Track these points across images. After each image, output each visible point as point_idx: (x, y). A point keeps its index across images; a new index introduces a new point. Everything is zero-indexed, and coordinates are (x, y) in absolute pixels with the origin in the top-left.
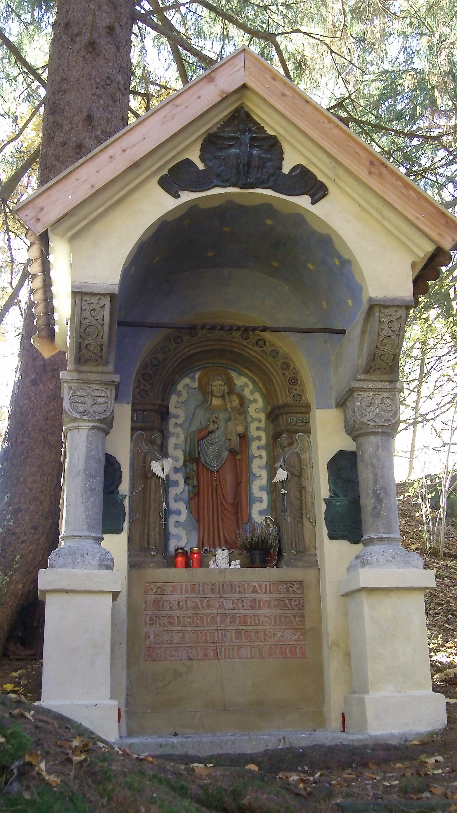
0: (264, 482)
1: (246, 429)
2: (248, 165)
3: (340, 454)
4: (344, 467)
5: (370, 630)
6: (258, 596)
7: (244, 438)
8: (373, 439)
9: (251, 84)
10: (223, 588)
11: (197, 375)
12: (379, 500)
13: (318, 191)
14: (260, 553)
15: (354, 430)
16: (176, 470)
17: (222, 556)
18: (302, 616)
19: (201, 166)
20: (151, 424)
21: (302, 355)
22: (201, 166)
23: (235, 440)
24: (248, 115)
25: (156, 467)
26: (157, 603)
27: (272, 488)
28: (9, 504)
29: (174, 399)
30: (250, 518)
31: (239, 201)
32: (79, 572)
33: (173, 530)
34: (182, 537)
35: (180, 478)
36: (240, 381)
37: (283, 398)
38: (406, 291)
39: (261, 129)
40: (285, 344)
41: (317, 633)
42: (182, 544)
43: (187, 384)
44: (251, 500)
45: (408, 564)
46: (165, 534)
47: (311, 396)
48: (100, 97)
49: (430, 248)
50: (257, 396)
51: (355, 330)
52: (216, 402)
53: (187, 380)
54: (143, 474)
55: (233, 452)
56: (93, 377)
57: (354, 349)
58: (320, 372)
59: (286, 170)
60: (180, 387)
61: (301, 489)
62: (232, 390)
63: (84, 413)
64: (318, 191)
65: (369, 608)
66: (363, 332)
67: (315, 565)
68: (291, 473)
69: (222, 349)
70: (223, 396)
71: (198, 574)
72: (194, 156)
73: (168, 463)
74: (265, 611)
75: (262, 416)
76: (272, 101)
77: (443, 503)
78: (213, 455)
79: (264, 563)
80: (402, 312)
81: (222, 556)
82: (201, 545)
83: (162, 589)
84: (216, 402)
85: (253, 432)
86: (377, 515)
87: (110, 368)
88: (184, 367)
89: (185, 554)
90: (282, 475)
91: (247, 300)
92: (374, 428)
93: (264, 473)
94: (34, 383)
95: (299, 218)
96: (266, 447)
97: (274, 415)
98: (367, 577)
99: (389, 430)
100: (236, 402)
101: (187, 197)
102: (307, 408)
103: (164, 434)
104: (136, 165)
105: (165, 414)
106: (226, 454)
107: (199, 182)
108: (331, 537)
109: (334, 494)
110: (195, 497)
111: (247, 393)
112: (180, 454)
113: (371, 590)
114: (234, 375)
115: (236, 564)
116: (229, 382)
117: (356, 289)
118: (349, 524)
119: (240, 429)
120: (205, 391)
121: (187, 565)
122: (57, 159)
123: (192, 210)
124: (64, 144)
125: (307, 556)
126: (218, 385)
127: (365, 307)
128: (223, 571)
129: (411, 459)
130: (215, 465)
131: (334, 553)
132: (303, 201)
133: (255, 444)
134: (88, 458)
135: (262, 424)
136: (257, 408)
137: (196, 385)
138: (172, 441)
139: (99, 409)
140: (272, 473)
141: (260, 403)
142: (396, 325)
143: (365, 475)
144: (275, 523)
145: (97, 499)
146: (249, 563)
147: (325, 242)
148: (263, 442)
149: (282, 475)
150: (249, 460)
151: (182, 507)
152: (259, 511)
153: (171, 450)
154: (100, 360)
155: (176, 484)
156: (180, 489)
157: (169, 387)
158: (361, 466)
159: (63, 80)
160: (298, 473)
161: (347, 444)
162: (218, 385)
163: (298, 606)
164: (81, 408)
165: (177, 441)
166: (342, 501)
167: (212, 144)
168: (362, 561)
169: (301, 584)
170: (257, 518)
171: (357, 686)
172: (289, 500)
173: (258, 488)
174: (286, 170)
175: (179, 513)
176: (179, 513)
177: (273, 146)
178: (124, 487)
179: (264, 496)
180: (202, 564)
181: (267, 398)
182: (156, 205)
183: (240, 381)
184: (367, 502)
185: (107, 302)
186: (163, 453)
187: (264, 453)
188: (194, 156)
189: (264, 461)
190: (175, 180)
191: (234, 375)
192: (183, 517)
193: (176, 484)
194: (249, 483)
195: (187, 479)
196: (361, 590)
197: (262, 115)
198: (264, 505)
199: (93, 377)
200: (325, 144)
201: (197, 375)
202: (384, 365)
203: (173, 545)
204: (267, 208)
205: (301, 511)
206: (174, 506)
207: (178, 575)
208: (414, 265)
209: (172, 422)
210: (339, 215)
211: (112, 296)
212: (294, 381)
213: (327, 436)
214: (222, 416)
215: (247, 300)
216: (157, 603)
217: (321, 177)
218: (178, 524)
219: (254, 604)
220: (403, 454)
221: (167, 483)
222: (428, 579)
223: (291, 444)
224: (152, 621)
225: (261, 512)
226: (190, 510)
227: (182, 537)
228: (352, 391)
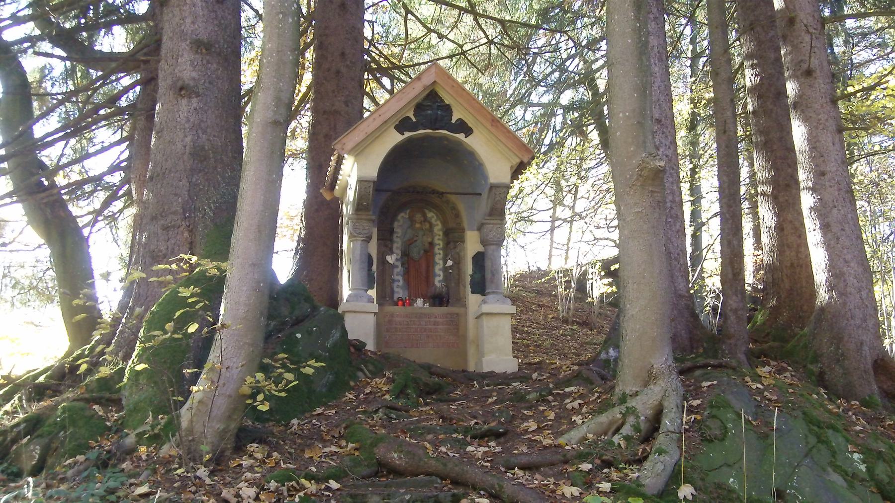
0: (441, 266)
1: (433, 239)
2: (436, 119)
3: (478, 253)
4: (479, 259)
5: (486, 331)
6: (437, 320)
7: (431, 244)
8: (493, 247)
9: (437, 80)
10: (420, 316)
11: (408, 211)
12: (493, 275)
13: (468, 131)
14: (439, 300)
15: (484, 243)
16: (397, 260)
17: (420, 302)
18: (458, 329)
19: (414, 120)
20: (386, 238)
21: (461, 205)
22: (414, 120)
23: (427, 245)
24: (436, 94)
25: (389, 258)
26: (390, 322)
27: (445, 269)
28: (306, 276)
29: (396, 224)
30: (434, 284)
31: (431, 137)
32: (361, 304)
33: (396, 289)
34: (400, 292)
35: (399, 264)
36: (430, 215)
37: (451, 225)
38: (506, 179)
39: (442, 101)
40: (453, 198)
41: (464, 337)
42: (401, 296)
43: (403, 216)
44: (435, 275)
45: (504, 303)
46: (392, 292)
47: (465, 224)
48: (349, 40)
49: (518, 161)
50: (439, 222)
51: (485, 195)
52: (418, 225)
53: (402, 214)
54: (382, 262)
55: (426, 251)
56: (364, 217)
57: (484, 205)
58: (470, 213)
59: (453, 121)
60: (399, 217)
61: (459, 269)
62: (426, 220)
63: (360, 233)
64: (468, 131)
65: (485, 321)
66: (488, 198)
67: (465, 306)
68: (454, 263)
69: (421, 199)
70: (421, 223)
71: (408, 309)
72: (411, 115)
73: (394, 257)
74: (441, 327)
75: (441, 233)
76: (446, 88)
77: (573, 285)
78: (415, 253)
79: (441, 304)
80: (505, 190)
81: (420, 302)
82: (410, 297)
83: (392, 315)
84: (418, 225)
85: (436, 241)
86: (492, 282)
87: (371, 213)
88: (402, 208)
89: (402, 300)
90: (450, 263)
91: (434, 177)
92: (494, 241)
93: (441, 262)
94: (317, 211)
95: (460, 143)
96: (443, 249)
97: (447, 233)
98: (486, 308)
99: (499, 243)
100: (427, 226)
101: (407, 134)
102: (463, 230)
103: (391, 241)
104: (386, 122)
105: (392, 231)
106: (422, 252)
107: (413, 127)
108: (473, 293)
109: (474, 272)
110: (406, 274)
111: (433, 221)
112: (399, 252)
113: (488, 314)
114: (427, 211)
115: (427, 305)
116: (424, 215)
117: (486, 177)
118: (480, 286)
119: (430, 240)
120: (411, 219)
121: (404, 305)
122: (325, 79)
123: (409, 140)
124: (329, 70)
125: (461, 302)
126: (418, 217)
127: (489, 186)
128: (421, 308)
129: (567, 250)
130: (416, 257)
131: (473, 300)
132: (461, 136)
133: (436, 248)
134: (361, 255)
135: (441, 237)
136: (438, 229)
137: (407, 216)
138: (395, 246)
139: (365, 232)
140: (445, 262)
141: (440, 226)
142: (502, 196)
143: (488, 264)
144: (446, 286)
145: (365, 273)
146: (433, 305)
147: (471, 155)
148: (441, 246)
149: (450, 263)
150: (434, 255)
151: (400, 278)
152: (438, 281)
153: (395, 250)
154: (366, 209)
155: (397, 267)
156: (399, 269)
157: (394, 218)
158: (486, 259)
159: (326, 27)
160: (458, 262)
161: (480, 249)
162: (418, 217)
163: (456, 325)
164: (358, 231)
165: (397, 245)
166: (477, 276)
167: (419, 108)
168: (484, 302)
169: (457, 314)
170: (438, 284)
171: (480, 354)
172: (453, 275)
173: (438, 269)
174: (453, 121)
175: (399, 281)
176: (399, 281)
177: (448, 109)
178: (374, 267)
179: (441, 273)
180: (410, 305)
181: (444, 223)
182: (394, 138)
183: (430, 215)
184: (488, 276)
185: (372, 184)
186: (391, 252)
187: (441, 252)
188: (411, 115)
189: (441, 256)
190: (403, 126)
191: (427, 211)
192: (401, 283)
193: (397, 267)
194: (433, 267)
195: (403, 264)
196: (483, 314)
197: (442, 94)
198: (441, 278)
199: (364, 217)
200: (471, 111)
201: (408, 211)
202: (498, 212)
203: (396, 296)
204: (445, 138)
205: (459, 280)
206: (396, 277)
207: (399, 309)
208: (512, 167)
209: (395, 235)
210: (478, 143)
211: (374, 182)
212: (457, 216)
213: (472, 245)
214: (421, 233)
215: (434, 177)
216: (390, 322)
217: (470, 125)
218: (398, 287)
219: (436, 323)
220: (560, 246)
221: (393, 266)
222: (513, 309)
223: (455, 248)
224: (388, 330)
225: (439, 281)
226: (404, 280)
227: (400, 292)
228: (483, 224)
